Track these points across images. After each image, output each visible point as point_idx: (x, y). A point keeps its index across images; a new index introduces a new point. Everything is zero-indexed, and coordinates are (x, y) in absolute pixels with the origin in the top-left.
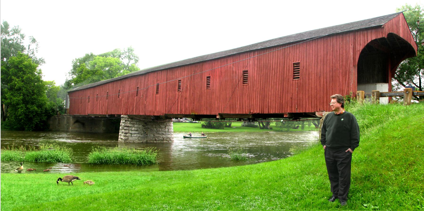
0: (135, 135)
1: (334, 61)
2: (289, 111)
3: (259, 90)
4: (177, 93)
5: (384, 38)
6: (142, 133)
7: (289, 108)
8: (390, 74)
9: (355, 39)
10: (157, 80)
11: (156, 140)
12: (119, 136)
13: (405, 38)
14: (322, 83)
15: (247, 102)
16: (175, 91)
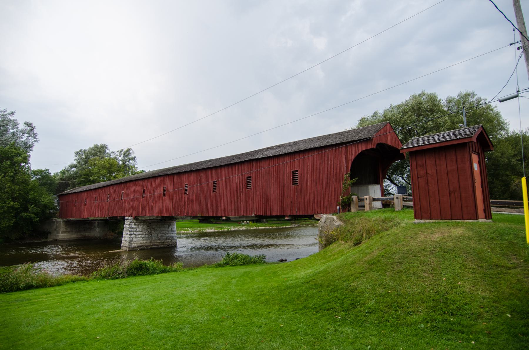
0: (140, 236)
2: (290, 214)
4: (184, 196)
5: (373, 148)
7: (289, 211)
10: (164, 184)
11: (159, 240)
12: (123, 239)
13: (394, 145)
14: (319, 189)
16: (182, 194)
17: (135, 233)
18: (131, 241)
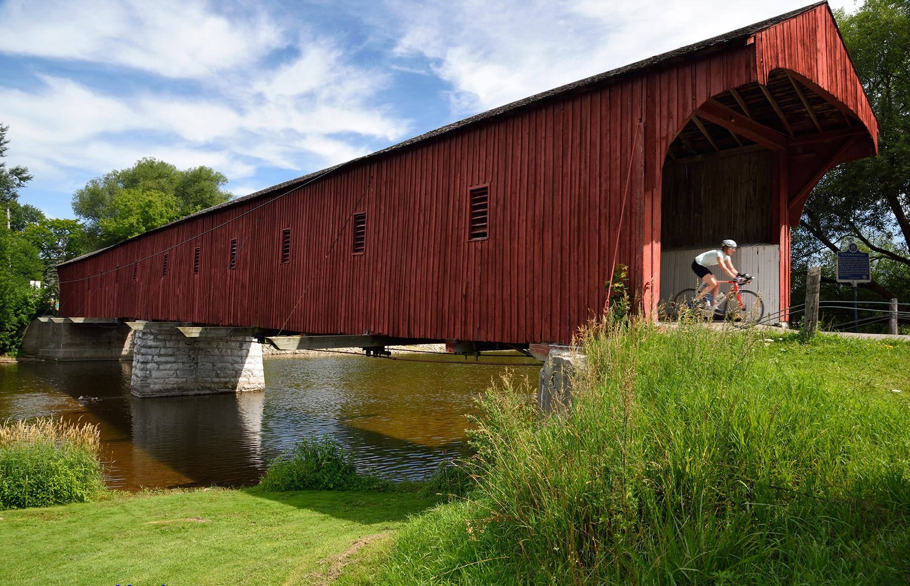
0: (168, 366)
1: (585, 177)
2: (458, 336)
3: (388, 269)
4: (229, 271)
6: (185, 360)
7: (458, 326)
8: (784, 213)
9: (653, 101)
11: (217, 376)
15: (361, 302)
17: (156, 358)
18: (146, 377)
